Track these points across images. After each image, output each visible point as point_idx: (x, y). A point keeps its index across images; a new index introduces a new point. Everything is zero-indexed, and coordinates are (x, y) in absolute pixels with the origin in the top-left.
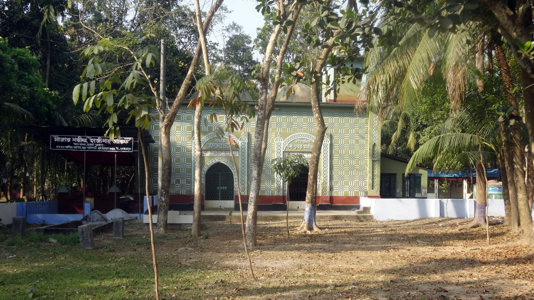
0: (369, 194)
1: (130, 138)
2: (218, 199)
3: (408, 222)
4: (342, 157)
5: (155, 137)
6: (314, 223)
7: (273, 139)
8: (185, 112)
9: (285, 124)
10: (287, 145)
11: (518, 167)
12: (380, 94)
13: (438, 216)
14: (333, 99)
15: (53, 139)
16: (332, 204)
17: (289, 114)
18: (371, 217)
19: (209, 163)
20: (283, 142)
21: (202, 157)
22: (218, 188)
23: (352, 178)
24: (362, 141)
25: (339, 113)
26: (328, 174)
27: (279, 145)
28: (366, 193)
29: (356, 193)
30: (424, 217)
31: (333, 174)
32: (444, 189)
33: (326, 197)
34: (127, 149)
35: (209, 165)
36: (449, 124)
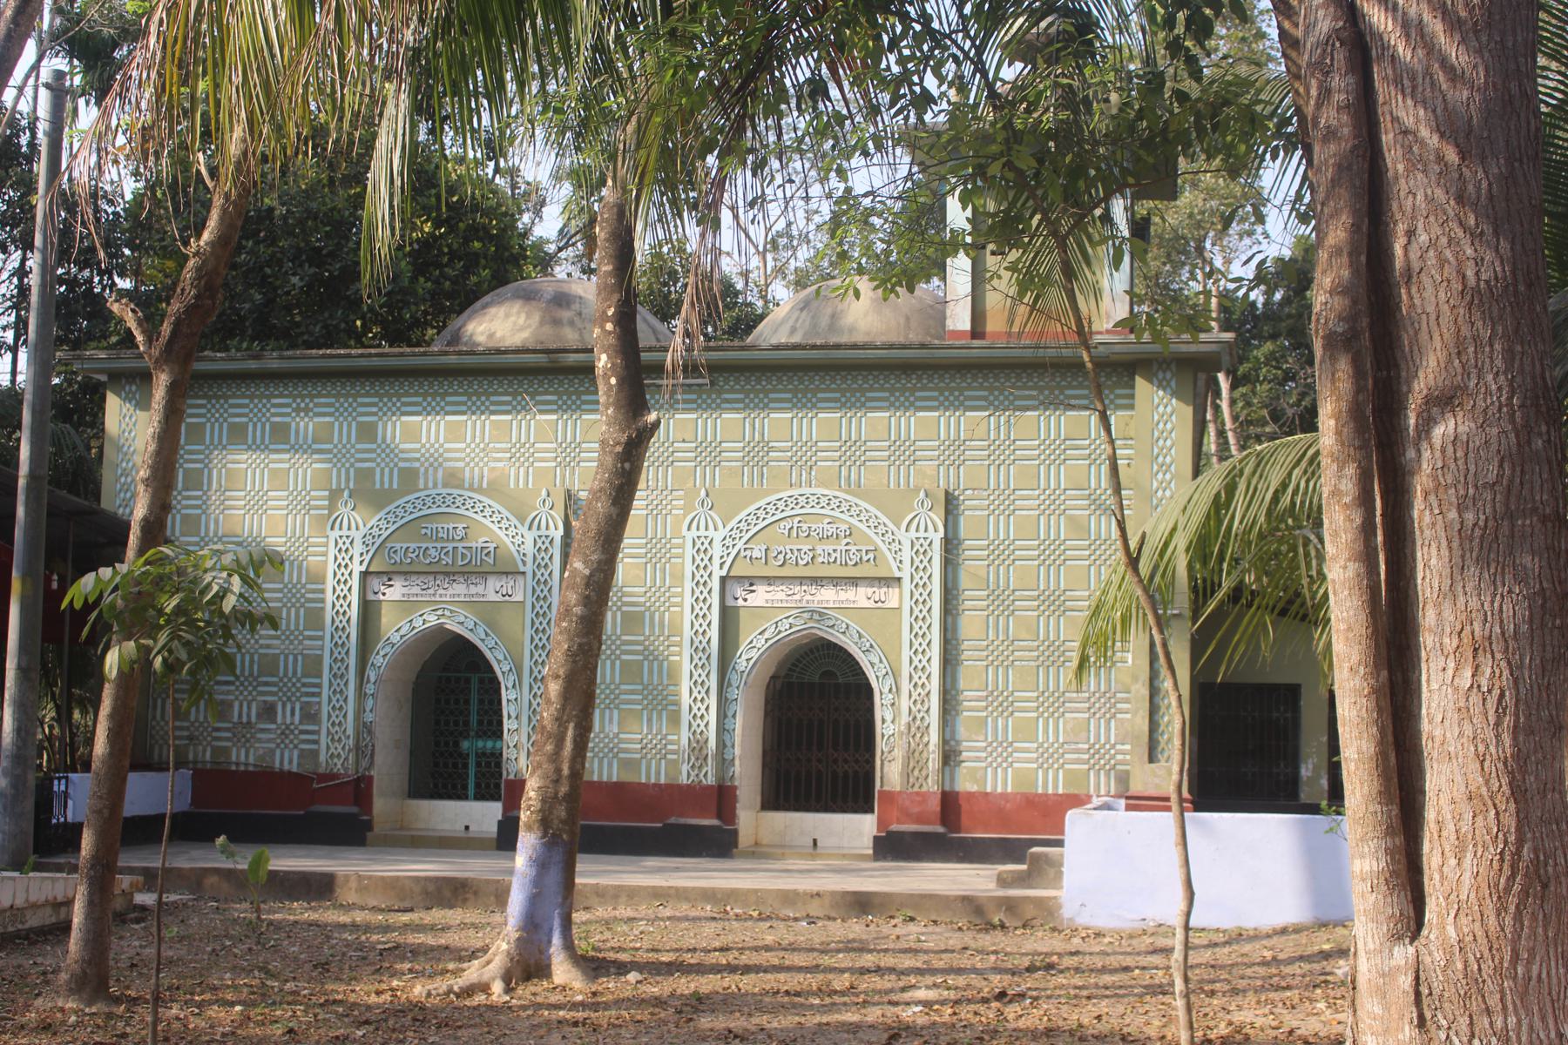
0: (1136, 787)
2: (463, 796)
3: (1239, 937)
4: (1002, 602)
5: (186, 518)
6: (556, 940)
7: (678, 522)
8: (307, 410)
9: (733, 452)
10: (740, 545)
12: (206, 236)
14: (967, 326)
16: (946, 830)
17: (851, 401)
18: (1048, 909)
19: (397, 629)
20: (722, 532)
21: (369, 610)
22: (465, 745)
25: (892, 391)
26: (935, 685)
28: (1123, 779)
30: (1325, 918)
31: (962, 684)
33: (924, 797)
35: (396, 638)
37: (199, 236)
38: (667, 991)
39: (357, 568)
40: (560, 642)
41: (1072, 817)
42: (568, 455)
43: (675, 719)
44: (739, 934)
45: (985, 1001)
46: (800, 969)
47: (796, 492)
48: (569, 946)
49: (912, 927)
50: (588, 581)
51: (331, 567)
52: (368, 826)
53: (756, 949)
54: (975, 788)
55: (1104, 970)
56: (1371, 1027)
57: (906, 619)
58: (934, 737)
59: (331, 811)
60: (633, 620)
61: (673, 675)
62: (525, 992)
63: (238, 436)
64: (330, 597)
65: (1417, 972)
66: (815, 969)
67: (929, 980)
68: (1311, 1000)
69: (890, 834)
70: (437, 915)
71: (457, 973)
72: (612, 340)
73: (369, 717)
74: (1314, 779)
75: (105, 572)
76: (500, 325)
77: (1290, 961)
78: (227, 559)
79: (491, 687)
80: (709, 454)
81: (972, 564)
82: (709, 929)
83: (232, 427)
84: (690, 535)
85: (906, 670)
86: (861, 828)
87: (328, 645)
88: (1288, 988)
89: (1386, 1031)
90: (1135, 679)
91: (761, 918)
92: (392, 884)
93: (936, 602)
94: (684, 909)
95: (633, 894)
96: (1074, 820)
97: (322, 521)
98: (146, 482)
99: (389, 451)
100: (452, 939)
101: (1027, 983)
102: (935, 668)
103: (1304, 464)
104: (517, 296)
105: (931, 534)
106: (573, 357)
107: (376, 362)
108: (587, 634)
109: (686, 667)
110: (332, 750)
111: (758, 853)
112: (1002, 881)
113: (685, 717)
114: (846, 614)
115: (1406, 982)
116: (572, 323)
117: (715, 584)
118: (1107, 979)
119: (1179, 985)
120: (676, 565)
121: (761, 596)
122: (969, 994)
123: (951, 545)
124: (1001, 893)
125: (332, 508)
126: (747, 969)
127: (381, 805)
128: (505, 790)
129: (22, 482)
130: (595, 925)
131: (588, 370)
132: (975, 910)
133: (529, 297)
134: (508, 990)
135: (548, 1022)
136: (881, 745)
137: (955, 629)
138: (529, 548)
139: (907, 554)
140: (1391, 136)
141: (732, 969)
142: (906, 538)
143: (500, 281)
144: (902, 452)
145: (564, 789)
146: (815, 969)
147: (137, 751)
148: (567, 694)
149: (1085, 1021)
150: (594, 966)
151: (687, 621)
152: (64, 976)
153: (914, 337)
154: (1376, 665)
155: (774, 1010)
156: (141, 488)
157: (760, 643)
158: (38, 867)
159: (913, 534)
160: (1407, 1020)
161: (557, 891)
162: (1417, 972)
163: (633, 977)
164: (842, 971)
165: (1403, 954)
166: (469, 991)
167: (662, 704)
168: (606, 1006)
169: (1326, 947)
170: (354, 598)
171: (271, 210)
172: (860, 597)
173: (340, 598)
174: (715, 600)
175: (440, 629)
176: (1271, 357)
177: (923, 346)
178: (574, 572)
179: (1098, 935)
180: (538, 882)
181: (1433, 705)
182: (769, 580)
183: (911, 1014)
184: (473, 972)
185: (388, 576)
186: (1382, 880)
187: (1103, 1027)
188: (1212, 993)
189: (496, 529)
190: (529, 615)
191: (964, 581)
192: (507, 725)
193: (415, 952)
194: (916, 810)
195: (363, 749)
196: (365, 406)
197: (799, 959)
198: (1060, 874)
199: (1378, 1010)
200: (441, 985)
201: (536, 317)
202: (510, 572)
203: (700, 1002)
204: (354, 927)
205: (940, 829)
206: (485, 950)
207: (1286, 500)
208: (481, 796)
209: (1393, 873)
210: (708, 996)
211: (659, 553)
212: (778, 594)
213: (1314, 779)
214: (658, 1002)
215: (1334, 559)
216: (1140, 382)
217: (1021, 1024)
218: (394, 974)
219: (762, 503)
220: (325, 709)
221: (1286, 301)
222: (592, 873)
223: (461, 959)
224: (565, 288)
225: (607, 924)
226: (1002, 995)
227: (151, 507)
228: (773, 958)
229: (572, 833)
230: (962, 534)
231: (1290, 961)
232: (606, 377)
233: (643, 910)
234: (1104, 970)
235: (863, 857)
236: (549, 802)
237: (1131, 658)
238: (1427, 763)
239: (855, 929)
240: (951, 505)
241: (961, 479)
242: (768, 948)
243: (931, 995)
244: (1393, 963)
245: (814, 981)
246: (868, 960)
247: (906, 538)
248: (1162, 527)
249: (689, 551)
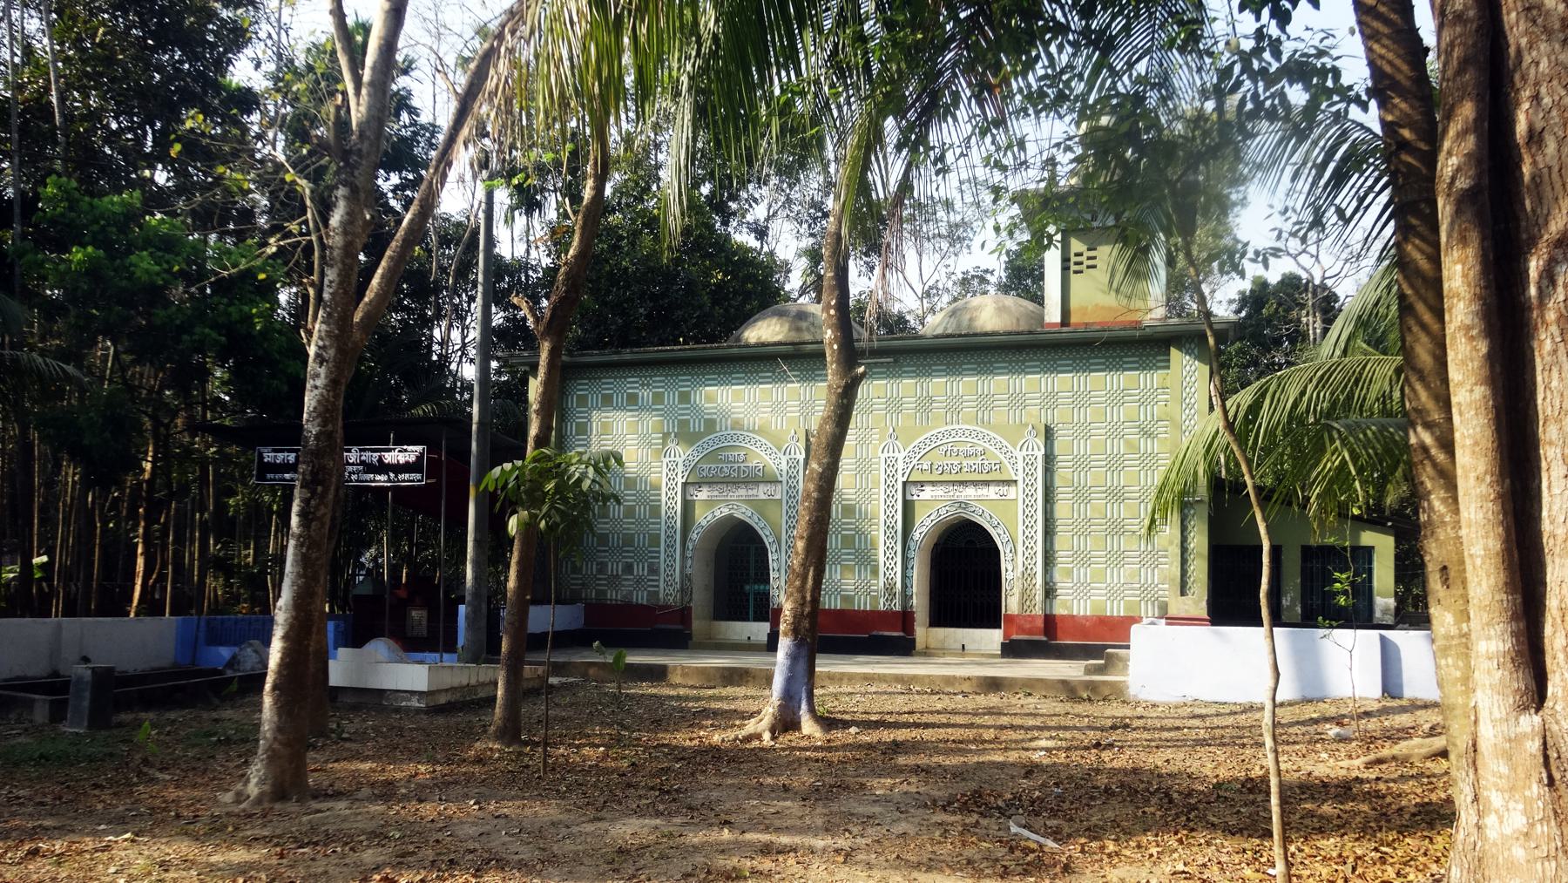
0: (1172, 612)
1: (419, 448)
2: (746, 619)
6: (804, 706)
7: (876, 448)
8: (648, 385)
9: (909, 403)
11: (1427, 438)
12: (571, 252)
13: (1377, 692)
16: (1046, 638)
17: (985, 369)
18: (1117, 693)
19: (704, 518)
20: (904, 454)
21: (688, 506)
22: (747, 587)
23: (1118, 558)
24: (1146, 445)
25: (1010, 362)
27: (891, 464)
28: (1164, 608)
29: (1129, 606)
30: (1309, 696)
31: (1057, 547)
32: (1345, 593)
33: (1033, 617)
34: (414, 476)
35: (704, 523)
37: (566, 253)
38: (875, 739)
39: (680, 481)
41: (1134, 628)
42: (806, 407)
43: (875, 572)
44: (919, 703)
45: (1086, 748)
46: (961, 726)
47: (949, 427)
48: (812, 710)
49: (1030, 699)
50: (821, 476)
51: (664, 480)
52: (690, 636)
53: (932, 713)
55: (1162, 729)
56: (1496, 785)
58: (1039, 580)
59: (669, 628)
60: (849, 510)
62: (785, 739)
63: (607, 402)
64: (664, 499)
65: (1545, 737)
66: (971, 726)
67: (1047, 734)
69: (1012, 641)
70: (729, 691)
71: (741, 727)
72: (834, 320)
73: (689, 571)
75: (508, 466)
76: (764, 331)
77: (1292, 724)
78: (585, 458)
79: (763, 552)
80: (895, 405)
81: (1062, 475)
82: (900, 700)
84: (883, 457)
85: (1020, 538)
86: (992, 638)
87: (663, 527)
88: (1295, 743)
89: (1512, 789)
90: (1171, 543)
91: (932, 693)
92: (703, 672)
94: (884, 687)
95: (851, 678)
97: (658, 452)
98: (537, 412)
99: (698, 410)
100: (740, 705)
101: (1114, 736)
102: (1040, 537)
104: (774, 314)
105: (1036, 452)
107: (689, 354)
109: (882, 538)
110: (667, 589)
111: (927, 653)
112: (1088, 671)
113: (882, 569)
114: (983, 505)
115: (1534, 746)
116: (808, 329)
117: (900, 487)
118: (1166, 735)
119: (1269, 742)
120: (871, 480)
121: (928, 493)
123: (1049, 459)
124: (1088, 678)
125: (664, 444)
126: (927, 726)
127: (697, 625)
128: (773, 616)
129: (474, 427)
130: (828, 696)
132: (1069, 690)
133: (781, 314)
134: (773, 738)
135: (799, 759)
138: (784, 466)
139: (1020, 465)
140: (1513, 15)
141: (917, 725)
142: (1020, 455)
145: (807, 610)
146: (971, 726)
147: (537, 587)
148: (808, 550)
150: (828, 723)
153: (1023, 327)
154: (1501, 474)
155: (949, 752)
156: (534, 416)
159: (1024, 452)
160: (1535, 777)
161: (803, 677)
162: (1545, 737)
163: (853, 730)
164: (989, 727)
165: (1530, 722)
166: (749, 738)
167: (865, 559)
168: (837, 749)
169: (1315, 716)
170: (679, 498)
172: (991, 492)
173: (670, 501)
175: (730, 517)
176: (1240, 352)
177: (1030, 333)
178: (812, 470)
179: (1154, 706)
180: (791, 669)
181: (1555, 508)
182: (933, 483)
183: (1036, 756)
184: (751, 727)
185: (699, 484)
186: (1508, 659)
187: (1172, 768)
188: (1244, 745)
189: (762, 456)
190: (785, 507)
191: (1058, 482)
192: (772, 575)
193: (716, 714)
194: (1028, 626)
195: (685, 590)
196: (683, 383)
197: (959, 719)
198: (1126, 667)
199: (1504, 769)
200: (730, 735)
201: (787, 326)
202: (776, 482)
204: (679, 698)
206: (759, 712)
208: (756, 619)
209: (1518, 653)
210: (902, 743)
211: (864, 467)
212: (939, 492)
214: (870, 747)
215: (1460, 384)
216: (1174, 352)
217: (1116, 764)
218: (701, 727)
220: (662, 566)
222: (826, 665)
223: (744, 718)
225: (836, 696)
226: (1097, 745)
227: (541, 428)
228: (943, 719)
231: (1292, 724)
232: (831, 344)
233: (858, 688)
234: (1162, 729)
235: (994, 656)
236: (798, 617)
238: (1548, 559)
240: (1049, 434)
241: (1057, 417)
242: (939, 712)
243: (1050, 744)
244: (1519, 730)
246: (1004, 720)
247: (1020, 455)
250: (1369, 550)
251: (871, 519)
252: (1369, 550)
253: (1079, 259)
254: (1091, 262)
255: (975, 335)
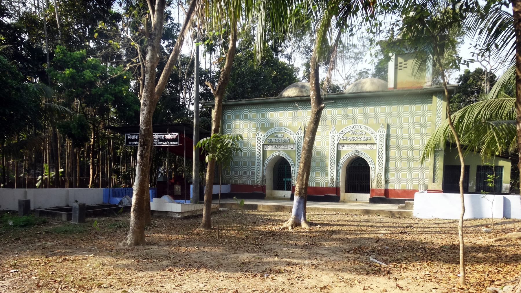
0: (430, 188)
1: (177, 134)
6: (302, 218)
8: (251, 111)
9: (340, 117)
10: (341, 137)
12: (225, 67)
13: (501, 216)
15: (127, 137)
16: (385, 197)
19: (270, 156)
21: (264, 152)
22: (284, 179)
24: (423, 131)
25: (375, 102)
26: (384, 166)
27: (333, 138)
28: (427, 187)
29: (414, 186)
30: (476, 217)
31: (390, 166)
32: (492, 182)
35: (270, 158)
36: (485, 79)
38: (326, 229)
39: (262, 144)
40: (303, 156)
43: (327, 174)
44: (341, 218)
46: (355, 226)
47: (353, 125)
48: (305, 220)
49: (379, 217)
51: (257, 143)
52: (265, 195)
53: (345, 221)
54: (392, 188)
55: (424, 228)
57: (377, 152)
58: (383, 177)
59: (259, 193)
60: (318, 154)
61: (327, 166)
62: (296, 229)
63: (238, 117)
64: (256, 150)
66: (358, 225)
67: (384, 229)
68: (478, 236)
69: (373, 198)
70: (278, 213)
72: (314, 88)
73: (265, 174)
74: (472, 187)
76: (290, 92)
77: (470, 227)
78: (230, 136)
79: (289, 168)
80: (334, 117)
81: (392, 141)
82: (335, 217)
83: (237, 115)
86: (367, 197)
87: (256, 159)
91: (345, 215)
92: (269, 207)
93: (384, 148)
94: (329, 212)
95: (318, 209)
96: (416, 195)
97: (255, 134)
98: (214, 121)
99: (268, 120)
101: (407, 230)
103: (485, 108)
104: (294, 86)
105: (383, 133)
106: (305, 98)
107: (265, 101)
108: (308, 153)
110: (257, 180)
111: (344, 201)
112: (399, 208)
113: (329, 173)
116: (305, 92)
117: (336, 145)
118: (425, 230)
120: (326, 143)
121: (346, 147)
122: (393, 232)
123: (388, 136)
124: (399, 210)
125: (256, 131)
126: (343, 225)
127: (268, 191)
129: (194, 126)
131: (309, 100)
132: (392, 214)
133: (296, 86)
134: (292, 229)
135: (300, 236)
136: (371, 179)
137: (388, 154)
138: (297, 139)
139: (378, 138)
141: (340, 225)
143: (290, 84)
144: (377, 115)
145: (304, 187)
146: (358, 225)
147: (215, 180)
149: (422, 239)
150: (310, 224)
151: (330, 154)
152: (202, 224)
153: (380, 89)
157: (345, 158)
158: (200, 203)
159: (379, 133)
161: (302, 209)
163: (319, 226)
164: (364, 226)
166: (284, 229)
167: (324, 170)
168: (313, 232)
169: (478, 224)
170: (261, 150)
171: (243, 72)
172: (367, 147)
173: (259, 151)
174: (336, 148)
175: (279, 156)
178: (306, 140)
179: (422, 220)
180: (298, 206)
182: (347, 144)
183: (380, 236)
184: (285, 225)
187: (427, 241)
188: (452, 234)
190: (297, 152)
191: (391, 144)
193: (273, 220)
195: (264, 180)
196: (263, 110)
200: (278, 227)
201: (298, 90)
202: (294, 144)
203: (333, 232)
204: (261, 215)
205: (384, 197)
206: (287, 220)
207: (479, 117)
208: (287, 190)
210: (335, 231)
211: (323, 138)
212: (349, 147)
213: (472, 187)
214: (324, 232)
217: (407, 239)
219: (346, 128)
220: (256, 172)
221: (462, 84)
222: (310, 205)
223: (282, 222)
224: (304, 84)
226: (401, 233)
228: (349, 223)
229: (306, 196)
230: (391, 133)
231: (470, 227)
233: (320, 213)
234: (424, 228)
236: (301, 189)
237: (429, 161)
239: (366, 217)
240: (388, 127)
241: (390, 121)
242: (347, 221)
243: (385, 232)
245: (358, 228)
246: (370, 224)
248: (445, 125)
249: (330, 138)
250: (502, 167)
251: (325, 156)
252: (502, 167)
253: (401, 65)
254: (405, 66)
255: (363, 92)
